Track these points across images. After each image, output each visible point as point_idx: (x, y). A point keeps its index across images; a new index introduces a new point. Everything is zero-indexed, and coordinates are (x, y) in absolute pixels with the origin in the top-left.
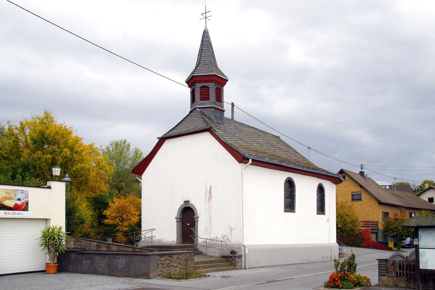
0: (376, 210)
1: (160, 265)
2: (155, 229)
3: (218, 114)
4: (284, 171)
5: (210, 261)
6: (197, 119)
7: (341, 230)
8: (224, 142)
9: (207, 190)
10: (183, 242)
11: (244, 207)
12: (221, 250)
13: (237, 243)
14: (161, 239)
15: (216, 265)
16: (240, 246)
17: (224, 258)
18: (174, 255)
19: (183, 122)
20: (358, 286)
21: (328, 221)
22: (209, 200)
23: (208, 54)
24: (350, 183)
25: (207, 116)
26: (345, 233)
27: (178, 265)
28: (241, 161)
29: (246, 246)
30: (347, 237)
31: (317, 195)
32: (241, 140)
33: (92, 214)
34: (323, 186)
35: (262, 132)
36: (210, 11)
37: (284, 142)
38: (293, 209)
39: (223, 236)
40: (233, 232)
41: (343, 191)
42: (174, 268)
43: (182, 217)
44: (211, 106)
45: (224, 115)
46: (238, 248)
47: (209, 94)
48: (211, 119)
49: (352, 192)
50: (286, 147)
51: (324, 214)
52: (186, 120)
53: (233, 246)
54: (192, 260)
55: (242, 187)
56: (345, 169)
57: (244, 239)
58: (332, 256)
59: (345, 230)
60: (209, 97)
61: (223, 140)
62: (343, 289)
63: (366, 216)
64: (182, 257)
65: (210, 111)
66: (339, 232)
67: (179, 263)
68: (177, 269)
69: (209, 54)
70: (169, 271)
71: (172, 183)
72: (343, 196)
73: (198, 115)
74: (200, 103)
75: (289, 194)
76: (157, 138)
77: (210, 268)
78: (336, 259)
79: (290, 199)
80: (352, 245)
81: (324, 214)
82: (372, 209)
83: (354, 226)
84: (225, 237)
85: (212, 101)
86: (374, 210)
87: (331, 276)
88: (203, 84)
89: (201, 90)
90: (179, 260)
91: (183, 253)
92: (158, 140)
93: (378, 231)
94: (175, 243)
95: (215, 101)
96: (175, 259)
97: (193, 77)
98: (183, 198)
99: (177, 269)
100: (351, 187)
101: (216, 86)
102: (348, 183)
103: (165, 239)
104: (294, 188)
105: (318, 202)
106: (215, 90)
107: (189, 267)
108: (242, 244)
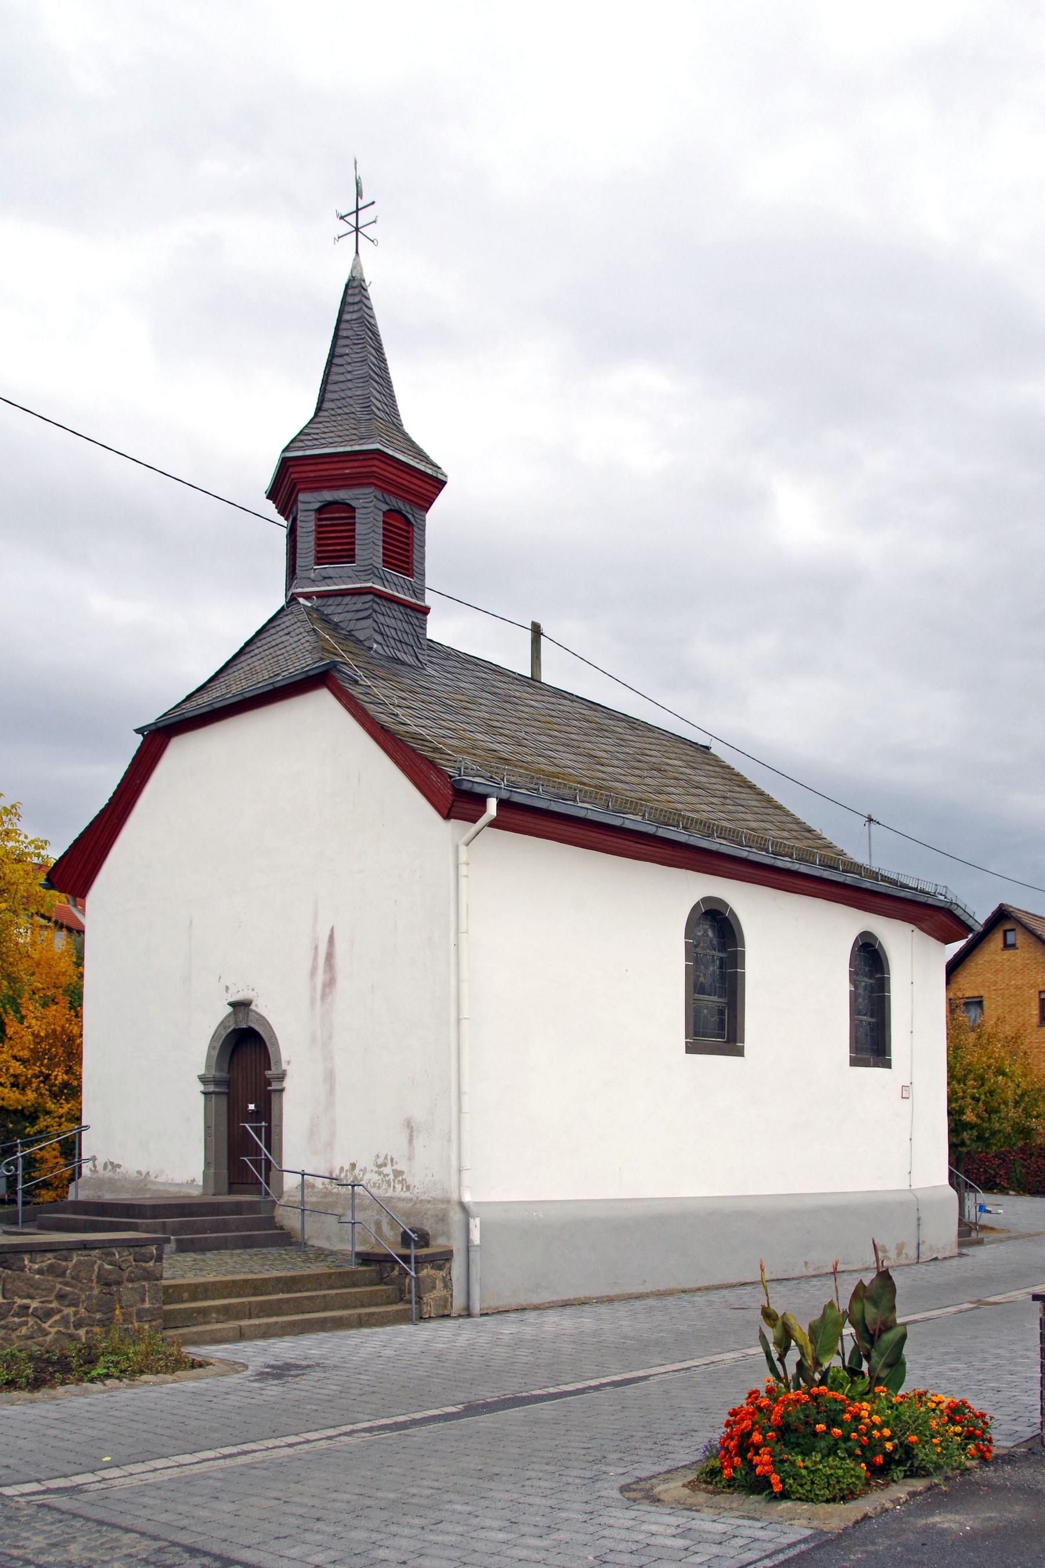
3: (392, 620)
4: (683, 871)
5: (278, 1279)
6: (292, 640)
7: (975, 1133)
8: (382, 727)
9: (316, 948)
10: (230, 1184)
11: (465, 1024)
12: (353, 1228)
13: (433, 1194)
14: (148, 1173)
15: (306, 1302)
16: (444, 1206)
17: (370, 1265)
19: (243, 658)
20: (898, 1473)
21: (906, 1092)
22: (323, 996)
23: (355, 373)
24: (1036, 959)
25: (342, 629)
26: (995, 1145)
27: (54, 1305)
28: (449, 806)
29: (473, 1209)
30: (1022, 1158)
31: (853, 981)
32: (491, 729)
34: (880, 944)
35: (623, 721)
36: (373, 203)
37: (728, 767)
38: (735, 1041)
39: (380, 1161)
40: (418, 1143)
41: (1008, 989)
42: (26, 1323)
43: (228, 1076)
44: (358, 586)
46: (436, 1216)
47: (353, 537)
48: (361, 641)
49: (1040, 992)
50: (730, 783)
51: (888, 1065)
52: (254, 647)
53: (418, 1206)
54: (145, 1279)
55: (457, 931)
56: (1014, 906)
57: (465, 1175)
58: (924, 1242)
59: (994, 1133)
60: (353, 550)
61: (384, 719)
62: (789, 1504)
64: (80, 1263)
65: (355, 608)
66: (968, 1142)
67: (61, 1297)
68: (46, 1326)
69: (359, 372)
71: (191, 923)
72: (1009, 1007)
73: (299, 624)
74: (312, 575)
75: (714, 972)
76: (138, 731)
77: (269, 1315)
78: (771, 1306)
79: (720, 996)
80: (1040, 1189)
81: (888, 1065)
83: (1029, 1116)
84: (385, 1165)
85: (366, 563)
87: (731, 1414)
88: (328, 496)
89: (320, 520)
90: (61, 1280)
91: (85, 1246)
92: (140, 738)
94: (196, 1192)
95: (380, 566)
96: (37, 1276)
97: (286, 462)
98: (227, 988)
99: (46, 1326)
100: (1037, 973)
101: (387, 504)
102: (1027, 955)
103: (162, 1172)
105: (855, 1011)
106: (381, 519)
107: (124, 1314)
108: (455, 1197)
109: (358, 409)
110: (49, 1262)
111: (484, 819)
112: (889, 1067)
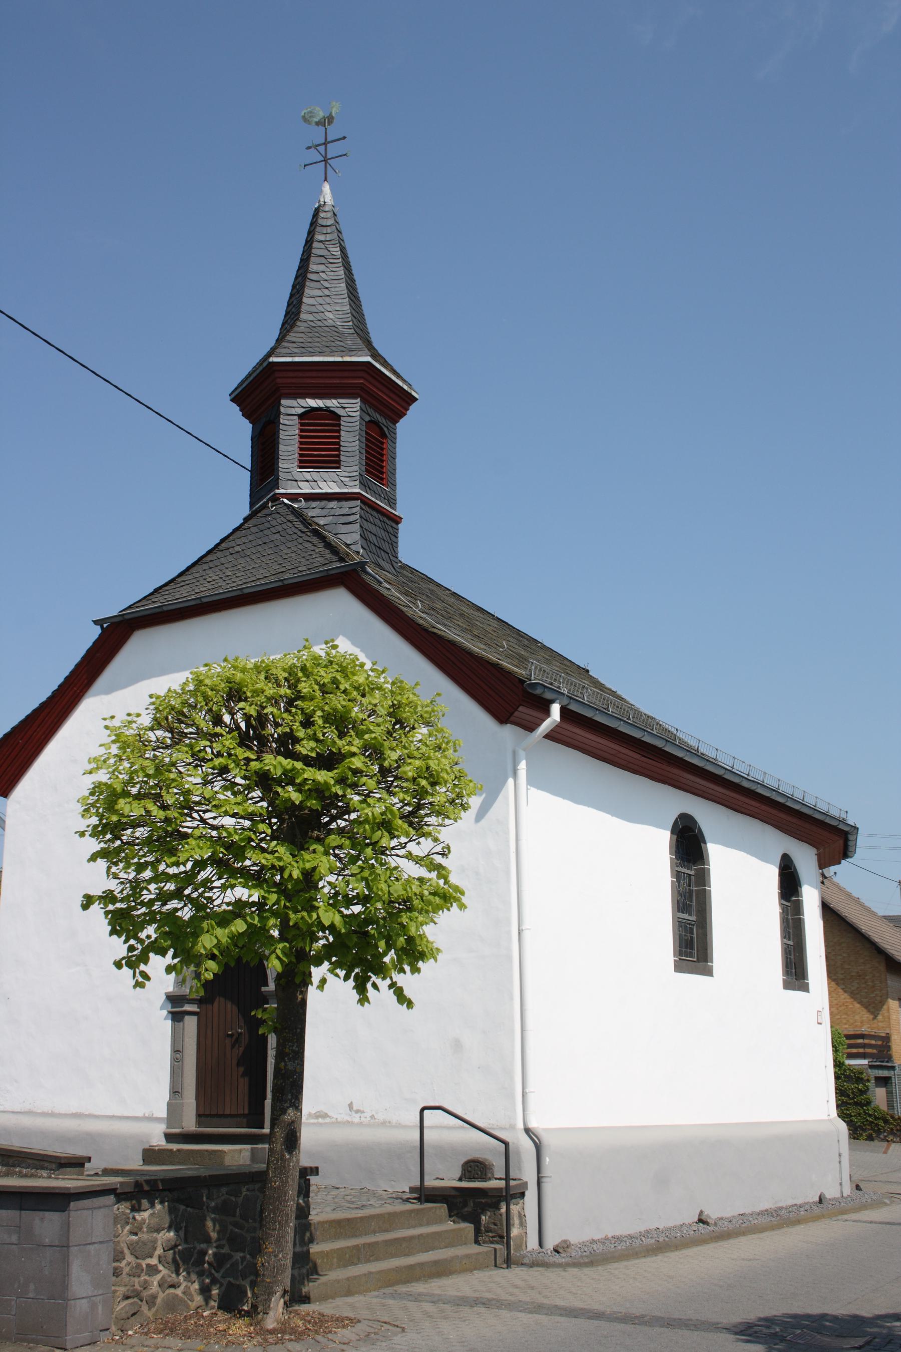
0: (878, 992)
1: (129, 1258)
2: (435, 923)
18: (205, 1192)
33: (184, 1273)
36: (344, 138)
45: (397, 537)
63: (846, 1014)
69: (337, 289)
70: (179, 1292)
76: (96, 622)
82: (865, 988)
86: (873, 992)
92: (97, 631)
93: (892, 1072)
101: (370, 415)
104: (704, 864)
109: (339, 323)
110: (223, 1198)
111: (546, 726)
112: (809, 992)
